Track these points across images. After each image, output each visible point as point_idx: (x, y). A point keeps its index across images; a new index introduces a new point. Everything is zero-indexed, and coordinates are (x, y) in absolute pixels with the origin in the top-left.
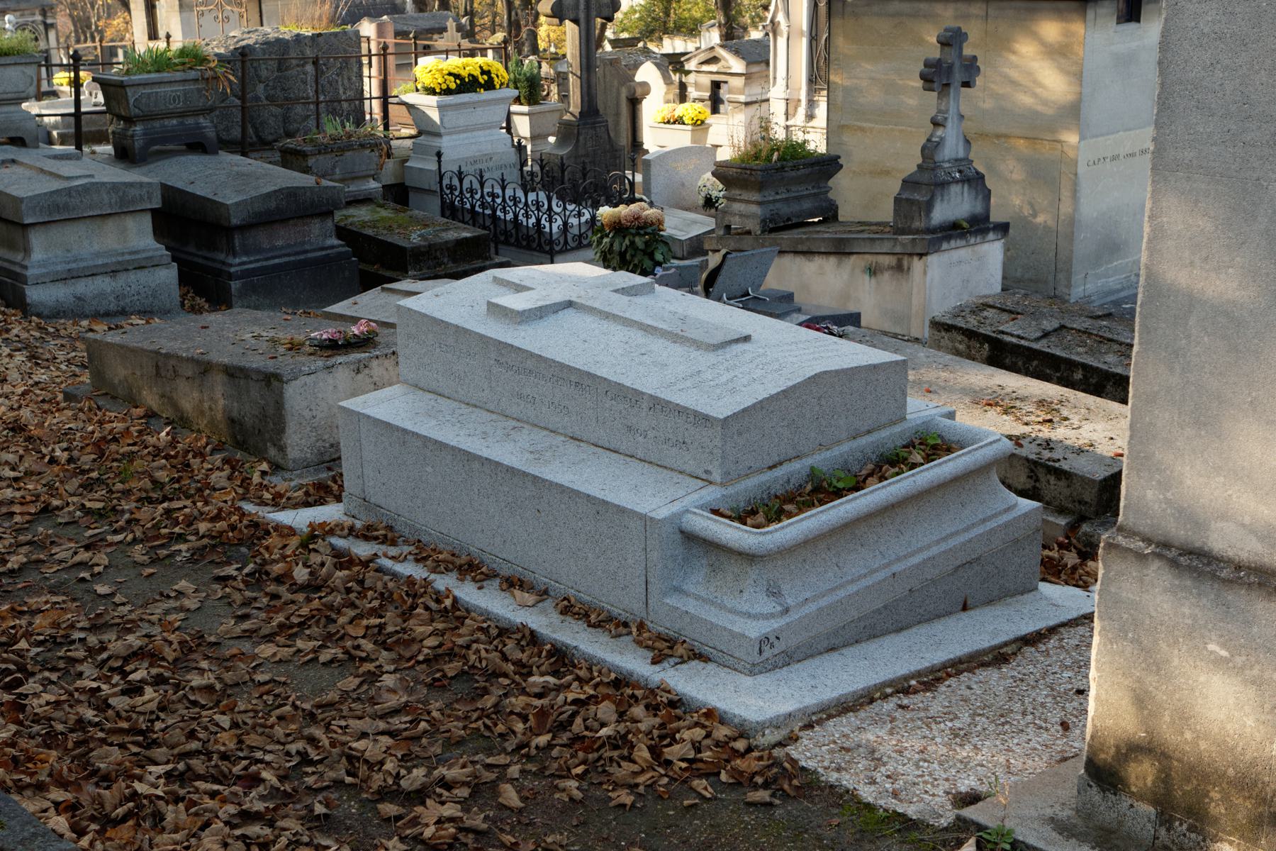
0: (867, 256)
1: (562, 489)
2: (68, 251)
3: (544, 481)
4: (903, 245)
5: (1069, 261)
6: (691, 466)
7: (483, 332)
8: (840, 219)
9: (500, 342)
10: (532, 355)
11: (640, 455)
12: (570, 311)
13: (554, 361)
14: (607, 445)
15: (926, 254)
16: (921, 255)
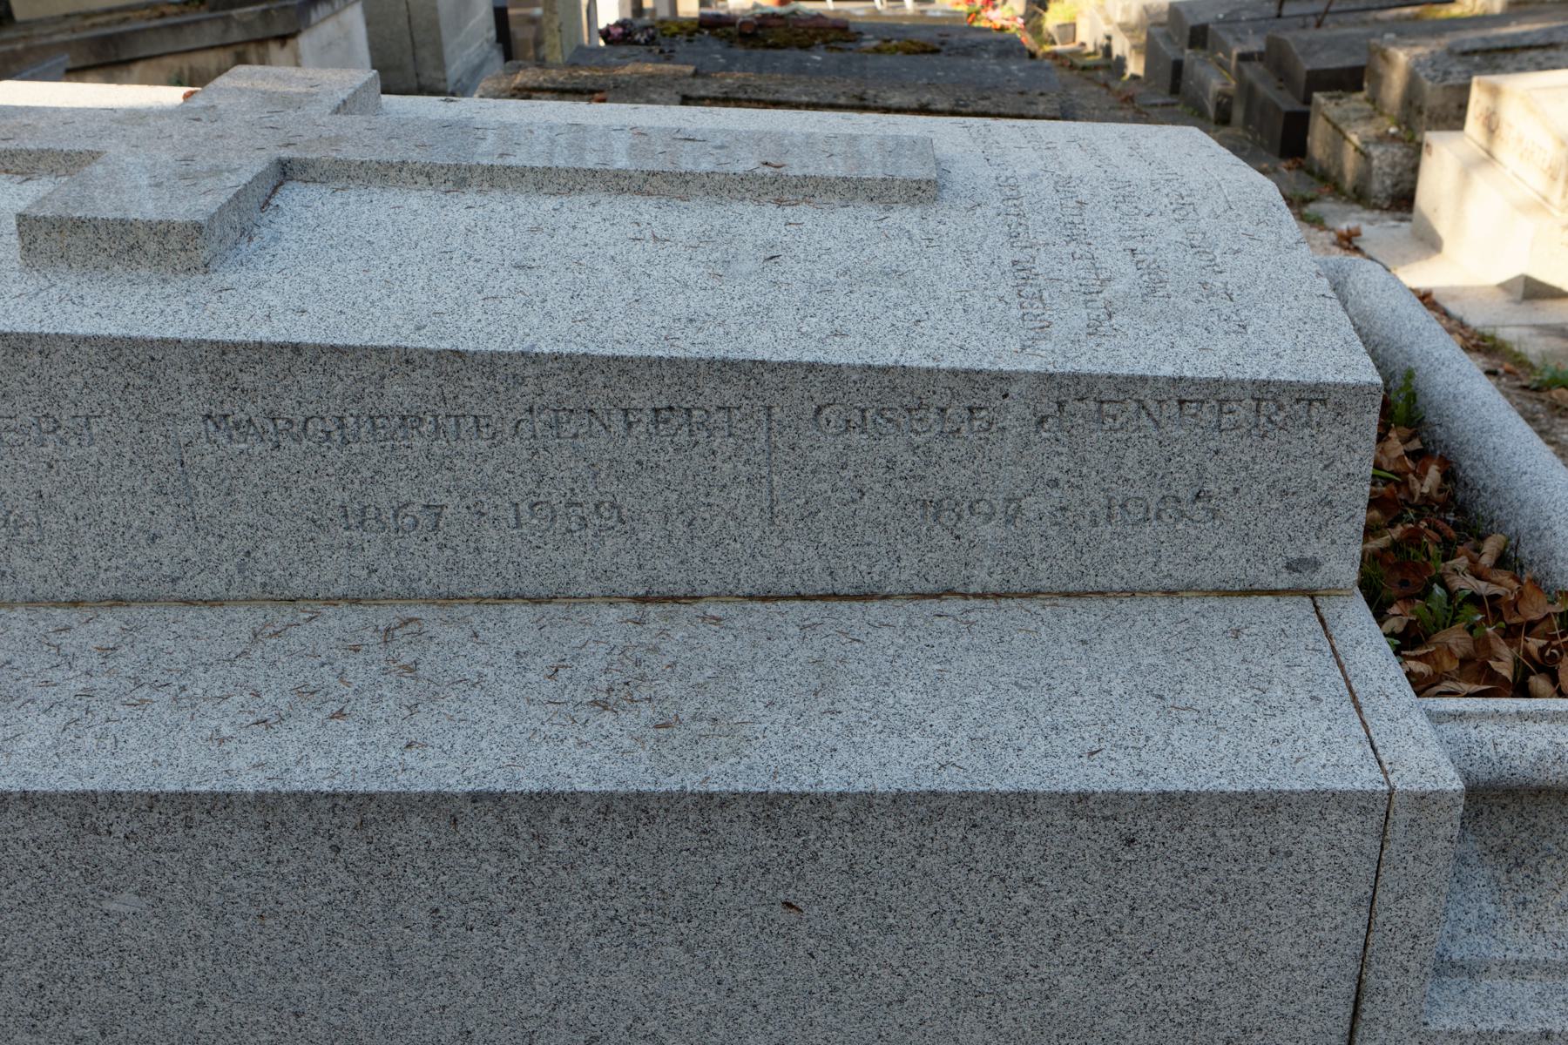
0: (168, 61)
1: (923, 809)
2: (1462, 860)
3: (820, 802)
4: (246, 26)
5: (434, 25)
6: (1232, 564)
7: (111, 328)
8: (20, 14)
9: (224, 349)
10: (408, 359)
11: (982, 578)
12: (294, 197)
13: (534, 358)
14: (822, 584)
15: (294, 35)
16: (283, 39)
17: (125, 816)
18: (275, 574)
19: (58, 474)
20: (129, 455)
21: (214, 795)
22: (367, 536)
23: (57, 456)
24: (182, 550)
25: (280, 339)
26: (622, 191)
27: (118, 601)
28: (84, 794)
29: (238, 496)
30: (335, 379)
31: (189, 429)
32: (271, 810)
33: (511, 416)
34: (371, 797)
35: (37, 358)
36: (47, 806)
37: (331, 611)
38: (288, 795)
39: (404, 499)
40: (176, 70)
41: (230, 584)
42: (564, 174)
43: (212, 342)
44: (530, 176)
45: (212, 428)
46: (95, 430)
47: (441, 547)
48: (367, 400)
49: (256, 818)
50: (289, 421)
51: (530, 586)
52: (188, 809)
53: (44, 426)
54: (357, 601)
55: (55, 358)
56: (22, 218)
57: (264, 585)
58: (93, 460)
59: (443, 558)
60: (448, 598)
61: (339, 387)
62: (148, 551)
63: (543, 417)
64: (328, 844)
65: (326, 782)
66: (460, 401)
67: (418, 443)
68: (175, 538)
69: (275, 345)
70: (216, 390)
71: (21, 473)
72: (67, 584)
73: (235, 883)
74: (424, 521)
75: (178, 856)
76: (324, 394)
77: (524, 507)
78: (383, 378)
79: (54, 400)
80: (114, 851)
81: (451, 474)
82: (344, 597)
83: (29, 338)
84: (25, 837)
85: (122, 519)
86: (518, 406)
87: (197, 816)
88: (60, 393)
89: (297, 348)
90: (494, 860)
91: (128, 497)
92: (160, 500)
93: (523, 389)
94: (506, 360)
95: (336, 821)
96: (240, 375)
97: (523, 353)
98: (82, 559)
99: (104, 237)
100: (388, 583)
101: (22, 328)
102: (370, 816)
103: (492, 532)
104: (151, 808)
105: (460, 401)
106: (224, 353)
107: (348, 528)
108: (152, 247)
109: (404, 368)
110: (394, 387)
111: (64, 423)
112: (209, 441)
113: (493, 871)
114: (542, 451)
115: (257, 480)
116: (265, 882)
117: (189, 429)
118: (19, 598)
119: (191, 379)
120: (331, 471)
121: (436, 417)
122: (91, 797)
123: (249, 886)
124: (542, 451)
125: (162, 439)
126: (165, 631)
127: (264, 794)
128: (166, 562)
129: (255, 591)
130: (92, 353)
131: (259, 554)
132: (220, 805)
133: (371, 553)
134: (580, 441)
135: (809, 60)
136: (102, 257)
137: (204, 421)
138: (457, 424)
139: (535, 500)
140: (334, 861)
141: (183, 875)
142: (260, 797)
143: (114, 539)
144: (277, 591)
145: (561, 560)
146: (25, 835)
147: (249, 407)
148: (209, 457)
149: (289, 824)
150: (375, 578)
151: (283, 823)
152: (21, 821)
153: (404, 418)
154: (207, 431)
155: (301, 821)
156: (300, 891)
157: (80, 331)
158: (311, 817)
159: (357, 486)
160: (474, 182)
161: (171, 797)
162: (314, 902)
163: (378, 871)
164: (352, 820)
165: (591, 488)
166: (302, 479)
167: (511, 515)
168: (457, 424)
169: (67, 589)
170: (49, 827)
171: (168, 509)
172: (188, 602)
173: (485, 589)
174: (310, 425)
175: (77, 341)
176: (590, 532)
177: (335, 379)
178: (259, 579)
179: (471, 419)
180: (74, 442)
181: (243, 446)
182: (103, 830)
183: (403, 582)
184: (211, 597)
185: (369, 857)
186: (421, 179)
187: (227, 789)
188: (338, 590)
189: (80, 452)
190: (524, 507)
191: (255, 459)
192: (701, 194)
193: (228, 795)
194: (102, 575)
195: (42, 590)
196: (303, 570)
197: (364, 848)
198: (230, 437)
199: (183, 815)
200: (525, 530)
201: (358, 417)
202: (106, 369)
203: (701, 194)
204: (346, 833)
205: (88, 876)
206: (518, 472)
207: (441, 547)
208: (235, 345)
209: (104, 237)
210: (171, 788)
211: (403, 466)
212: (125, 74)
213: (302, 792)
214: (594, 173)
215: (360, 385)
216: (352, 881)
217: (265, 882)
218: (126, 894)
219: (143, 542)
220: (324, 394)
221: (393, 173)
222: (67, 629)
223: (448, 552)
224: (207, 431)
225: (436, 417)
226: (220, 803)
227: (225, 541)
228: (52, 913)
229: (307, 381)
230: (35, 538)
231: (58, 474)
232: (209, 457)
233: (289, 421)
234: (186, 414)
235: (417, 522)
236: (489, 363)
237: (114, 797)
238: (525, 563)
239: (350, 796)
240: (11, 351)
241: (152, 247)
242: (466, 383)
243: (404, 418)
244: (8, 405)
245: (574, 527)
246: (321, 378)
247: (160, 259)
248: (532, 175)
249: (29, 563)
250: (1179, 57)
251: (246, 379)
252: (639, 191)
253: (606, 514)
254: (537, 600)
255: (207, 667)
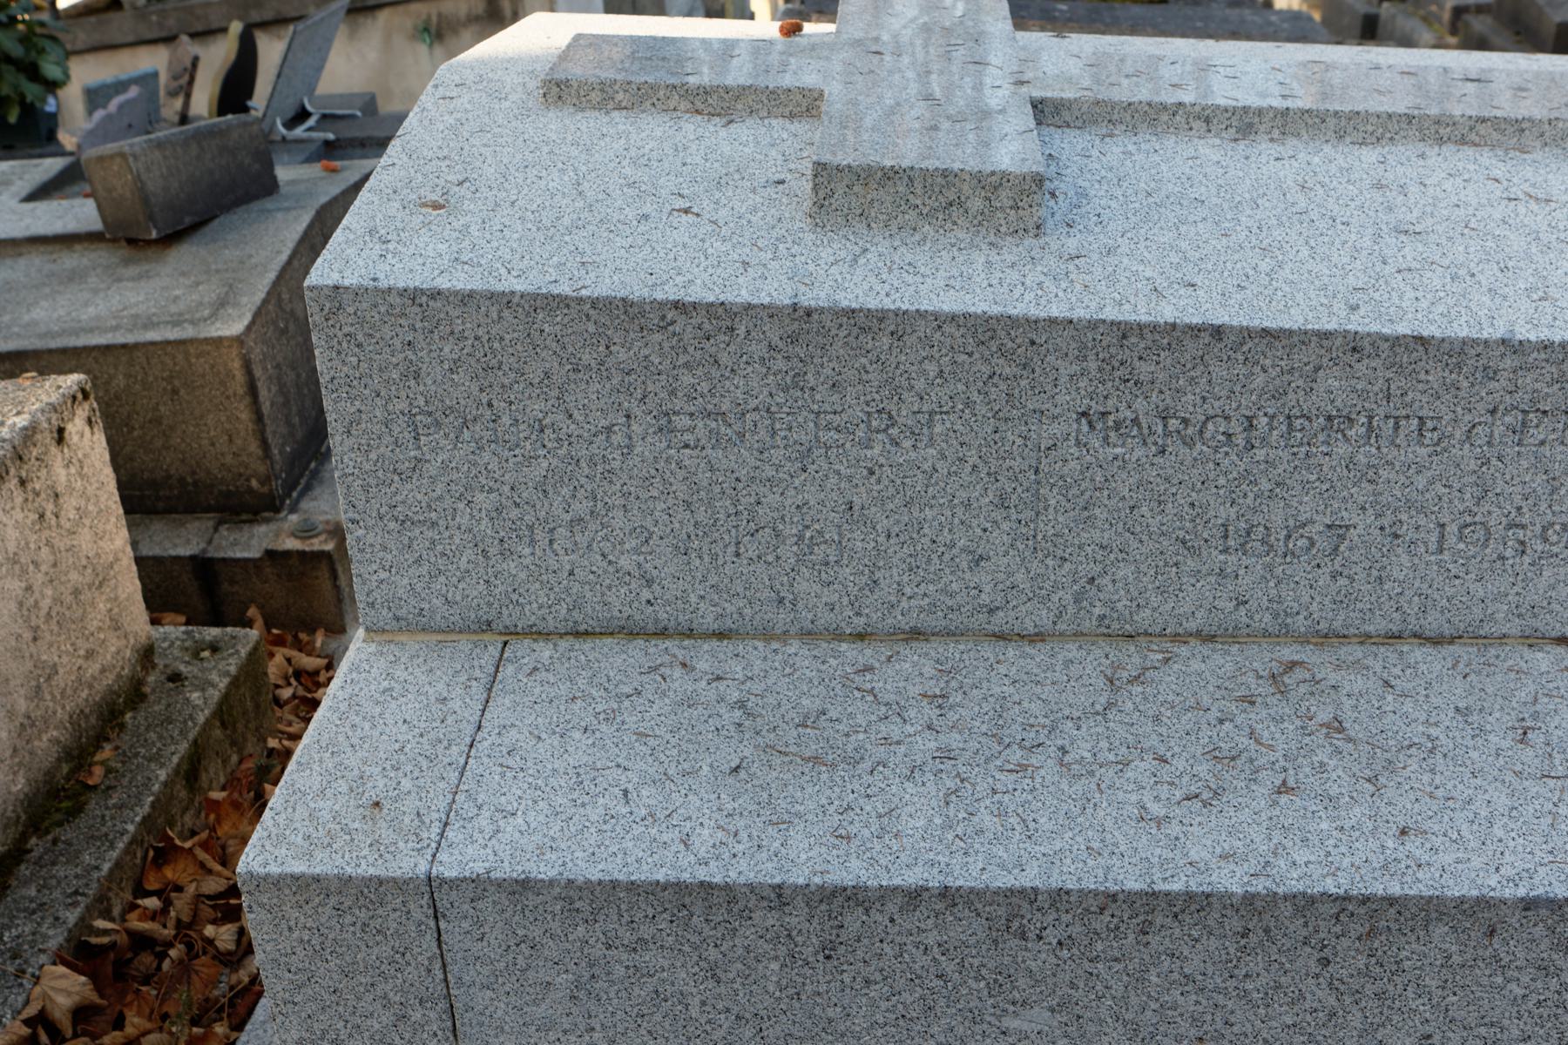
7: (979, 303)
9: (1124, 331)
10: (1355, 346)
17: (1066, 918)
18: (1119, 606)
19: (879, 481)
20: (974, 460)
21: (1190, 896)
22: (1245, 561)
23: (882, 460)
24: (1010, 574)
25: (1196, 320)
26: (1441, 141)
27: (916, 634)
28: (1022, 892)
29: (1097, 511)
30: (1257, 369)
31: (1057, 429)
32: (1256, 914)
33: (1468, 418)
34: (1391, 901)
35: (886, 340)
36: (969, 904)
37: (1184, 651)
38: (1285, 898)
39: (1302, 518)
40: (424, 17)
41: (1060, 616)
42: (1373, 120)
43: (1112, 323)
44: (1331, 122)
45: (1085, 428)
46: (938, 429)
47: (1335, 576)
48: (1291, 396)
49: (1236, 924)
50: (1185, 421)
51: (1433, 622)
52: (1149, 909)
53: (874, 423)
54: (1211, 638)
55: (910, 340)
56: (820, 168)
57: (1102, 617)
58: (926, 466)
59: (1334, 588)
60: (1326, 636)
61: (1260, 380)
62: (968, 575)
63: (1508, 419)
64: (1317, 955)
65: (1329, 880)
66: (1408, 399)
67: (1342, 449)
68: (1005, 560)
69: (1191, 327)
70: (1103, 382)
71: (833, 480)
72: (858, 614)
73: (1181, 1000)
74: (1323, 544)
75: (1117, 967)
76: (1238, 388)
77: (1452, 529)
78: (1317, 369)
79: (897, 392)
80: (1039, 959)
81: (1370, 488)
82: (1198, 634)
83: (881, 316)
84: (930, 941)
85: (946, 536)
86: (1480, 406)
87: (1159, 920)
88: (905, 384)
89: (1218, 332)
90: (1526, 979)
91: (960, 511)
92: (998, 515)
93: (1493, 385)
94: (1480, 349)
95: (1338, 929)
96: (1137, 363)
97: (1504, 341)
98: (883, 583)
99: (919, 191)
100: (1257, 618)
101: (872, 304)
102: (1383, 923)
103: (1405, 559)
104: (1102, 910)
105: (1408, 399)
106: (1124, 337)
107: (1225, 551)
108: (976, 204)
109: (1348, 358)
110: (1331, 381)
111: (901, 420)
112: (1078, 443)
113: (1519, 992)
114: (1494, 461)
115: (1126, 493)
116: (1221, 1000)
117: (1057, 429)
118: (793, 631)
119: (1075, 368)
120: (1222, 481)
121: (1370, 418)
122: (1030, 895)
123: (1197, 1003)
124: (1494, 461)
125: (1019, 441)
126: (1002, 672)
127: (1254, 896)
128: (987, 589)
129: (1088, 625)
130: (958, 334)
131: (1106, 580)
132: (1194, 907)
133: (1245, 581)
134: (1546, 450)
135: (1055, 10)
136: (912, 215)
137: (1078, 421)
138: (1397, 427)
139: (1469, 520)
140: (1317, 976)
141: (1118, 989)
142: (1249, 899)
143: (929, 560)
144: (1115, 625)
145: (1481, 593)
146: (931, 939)
147: (1140, 404)
148: (1073, 464)
149: (1274, 931)
150: (1242, 611)
151: (1267, 931)
152: (930, 922)
153: (1329, 418)
154: (1078, 431)
155: (1292, 928)
156: (1262, 1011)
157: (946, 308)
158: (1306, 924)
159: (1249, 501)
160: (1262, 128)
161: (1131, 898)
162: (1274, 1024)
163: (1369, 989)
164: (1357, 929)
165: (1543, 506)
166: (1184, 490)
167: (1434, 538)
168: (1397, 427)
169: (855, 620)
170: (967, 928)
171: (1005, 526)
172: (1001, 637)
173: (1377, 625)
174: (1210, 426)
175: (941, 320)
176: (1527, 560)
177: (1257, 369)
178: (1097, 611)
179: (1416, 421)
180: (907, 444)
181: (1118, 450)
182: (1031, 935)
183: (1276, 616)
184: (1032, 630)
185: (1366, 973)
186: (1196, 124)
187: (1207, 889)
188: (1192, 626)
189: (913, 455)
190: (1452, 529)
191: (1130, 467)
192: (1538, 144)
193: (1208, 896)
194: (904, 604)
195: (826, 618)
196: (1155, 601)
197: (1361, 961)
198: (1106, 439)
199: (1142, 918)
200: (1446, 556)
201: (1273, 417)
202: (970, 355)
203: (1538, 144)
204: (1345, 942)
205: (995, 988)
206: (1456, 486)
207: (1335, 576)
208: (1141, 327)
209: (919, 191)
210: (1133, 885)
211: (1315, 477)
212: (369, 21)
213: (1304, 894)
214: (1410, 118)
215: (1286, 377)
216: (1332, 1001)
217: (1221, 1000)
218: (1037, 1009)
219: (964, 565)
220: (1238, 388)
221: (1165, 117)
222: (869, 669)
223: (1342, 581)
224: (1078, 431)
225: (1370, 418)
226: (1196, 904)
227: (1067, 566)
228: (935, 1029)
229: (1219, 372)
230: (832, 559)
231: (879, 481)
232: (1073, 464)
233: (1185, 421)
234: (1058, 410)
235: (1312, 544)
236: (1455, 353)
237: (1059, 896)
238: (1436, 596)
239: (1365, 900)
240: (855, 331)
241: (976, 204)
242: (1422, 376)
243: (1329, 418)
244: (836, 397)
245: (1509, 553)
246: (1241, 370)
247: (981, 221)
248: (1334, 121)
249: (817, 588)
250: (1373, 10)
251: (1144, 369)
252: (1463, 141)
253: (1554, 538)
254: (1437, 641)
255: (1077, 722)
